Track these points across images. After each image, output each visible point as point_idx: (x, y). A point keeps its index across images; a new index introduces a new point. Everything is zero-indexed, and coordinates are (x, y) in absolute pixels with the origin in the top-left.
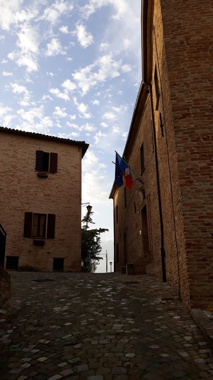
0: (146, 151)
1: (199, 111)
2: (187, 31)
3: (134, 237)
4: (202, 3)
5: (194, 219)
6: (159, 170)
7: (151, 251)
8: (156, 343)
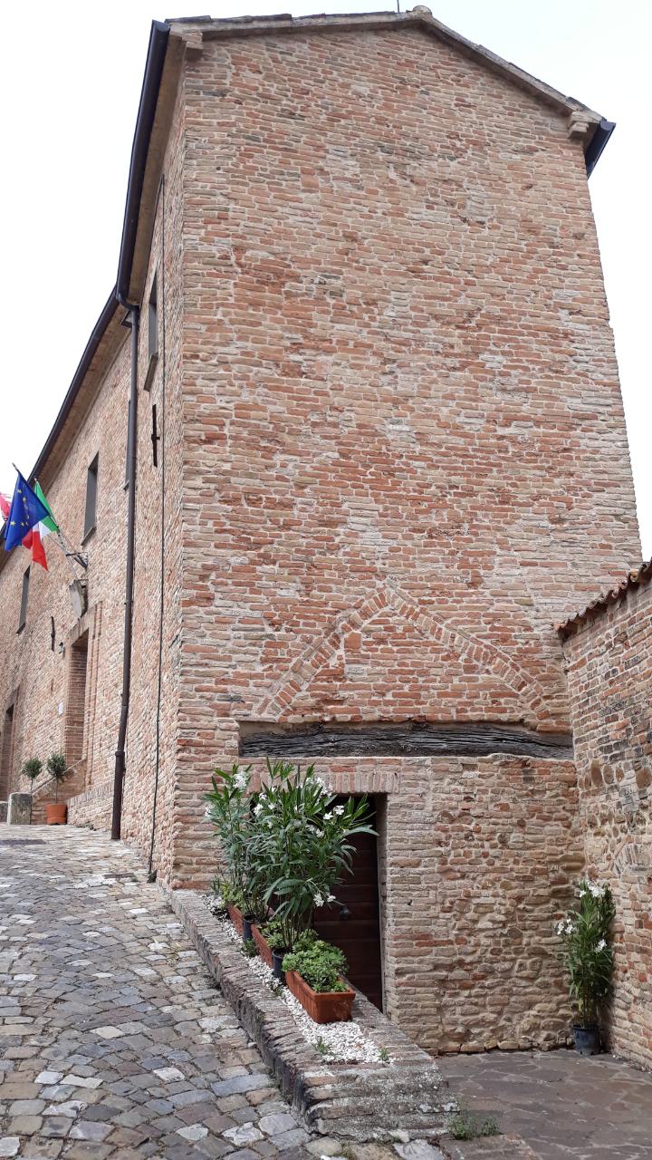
0: (104, 480)
1: (245, 434)
2: (240, 233)
3: (39, 720)
4: (282, 174)
5: (205, 684)
6: (137, 544)
7: (86, 760)
8: (84, 956)
